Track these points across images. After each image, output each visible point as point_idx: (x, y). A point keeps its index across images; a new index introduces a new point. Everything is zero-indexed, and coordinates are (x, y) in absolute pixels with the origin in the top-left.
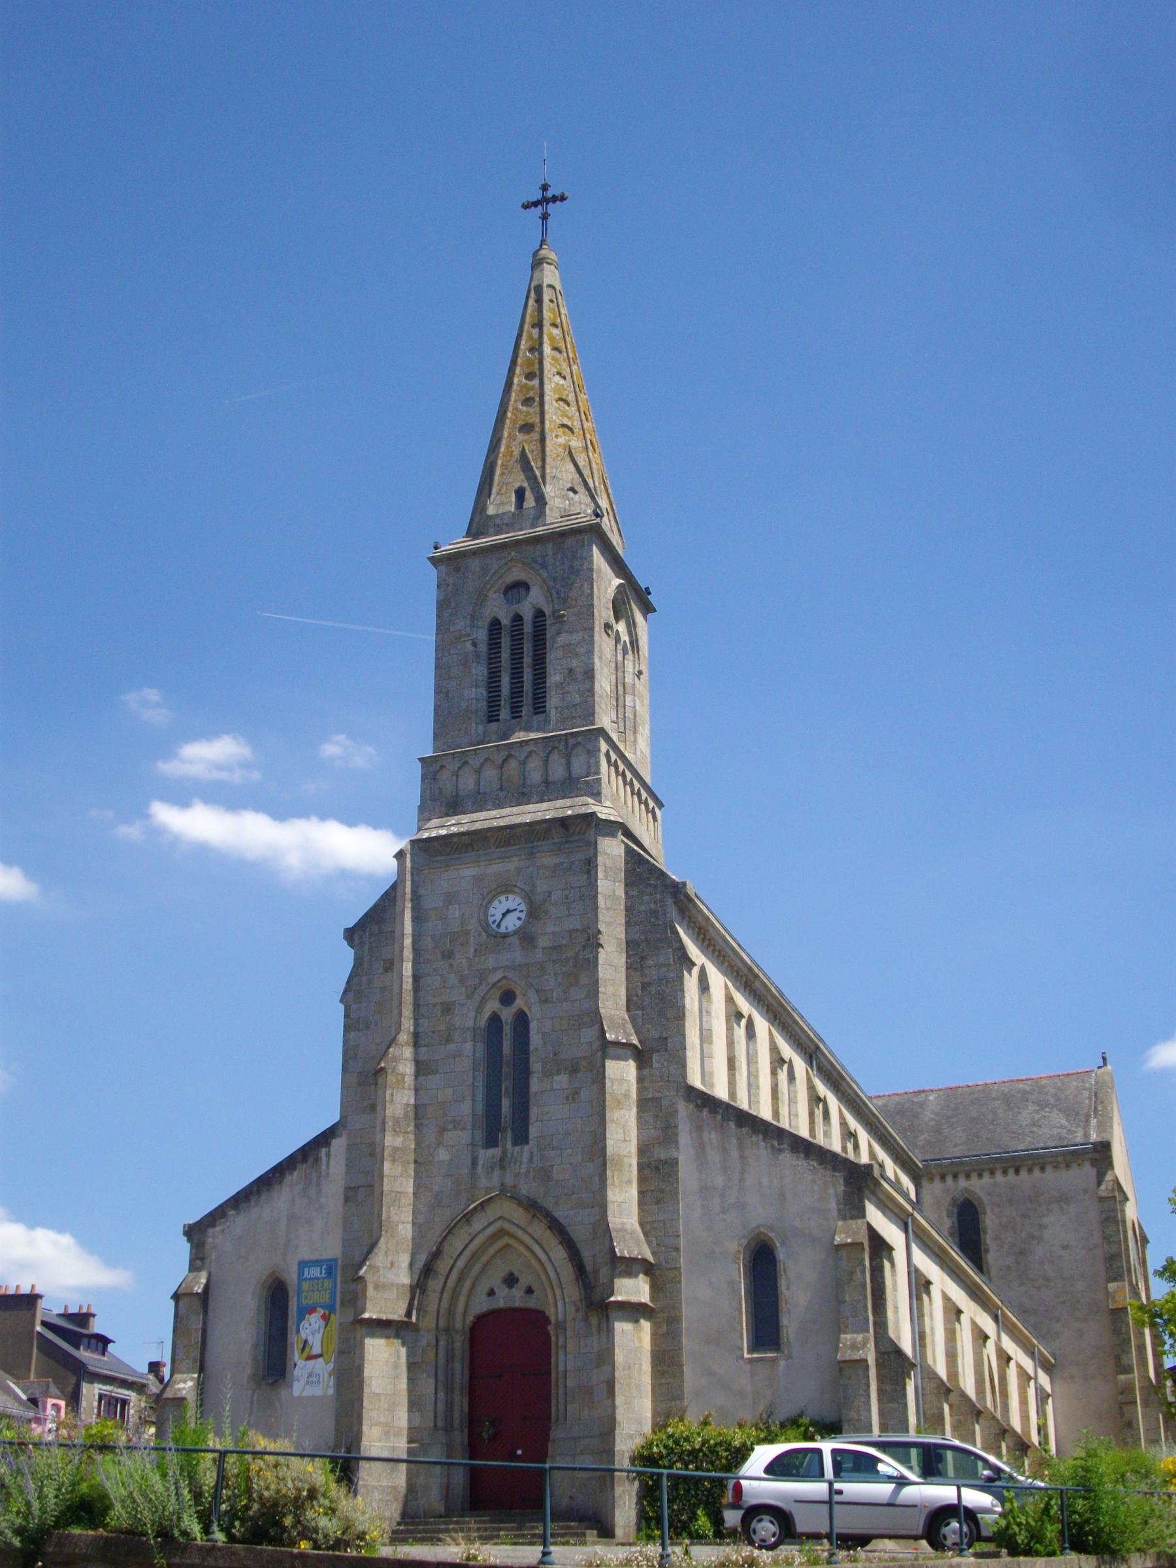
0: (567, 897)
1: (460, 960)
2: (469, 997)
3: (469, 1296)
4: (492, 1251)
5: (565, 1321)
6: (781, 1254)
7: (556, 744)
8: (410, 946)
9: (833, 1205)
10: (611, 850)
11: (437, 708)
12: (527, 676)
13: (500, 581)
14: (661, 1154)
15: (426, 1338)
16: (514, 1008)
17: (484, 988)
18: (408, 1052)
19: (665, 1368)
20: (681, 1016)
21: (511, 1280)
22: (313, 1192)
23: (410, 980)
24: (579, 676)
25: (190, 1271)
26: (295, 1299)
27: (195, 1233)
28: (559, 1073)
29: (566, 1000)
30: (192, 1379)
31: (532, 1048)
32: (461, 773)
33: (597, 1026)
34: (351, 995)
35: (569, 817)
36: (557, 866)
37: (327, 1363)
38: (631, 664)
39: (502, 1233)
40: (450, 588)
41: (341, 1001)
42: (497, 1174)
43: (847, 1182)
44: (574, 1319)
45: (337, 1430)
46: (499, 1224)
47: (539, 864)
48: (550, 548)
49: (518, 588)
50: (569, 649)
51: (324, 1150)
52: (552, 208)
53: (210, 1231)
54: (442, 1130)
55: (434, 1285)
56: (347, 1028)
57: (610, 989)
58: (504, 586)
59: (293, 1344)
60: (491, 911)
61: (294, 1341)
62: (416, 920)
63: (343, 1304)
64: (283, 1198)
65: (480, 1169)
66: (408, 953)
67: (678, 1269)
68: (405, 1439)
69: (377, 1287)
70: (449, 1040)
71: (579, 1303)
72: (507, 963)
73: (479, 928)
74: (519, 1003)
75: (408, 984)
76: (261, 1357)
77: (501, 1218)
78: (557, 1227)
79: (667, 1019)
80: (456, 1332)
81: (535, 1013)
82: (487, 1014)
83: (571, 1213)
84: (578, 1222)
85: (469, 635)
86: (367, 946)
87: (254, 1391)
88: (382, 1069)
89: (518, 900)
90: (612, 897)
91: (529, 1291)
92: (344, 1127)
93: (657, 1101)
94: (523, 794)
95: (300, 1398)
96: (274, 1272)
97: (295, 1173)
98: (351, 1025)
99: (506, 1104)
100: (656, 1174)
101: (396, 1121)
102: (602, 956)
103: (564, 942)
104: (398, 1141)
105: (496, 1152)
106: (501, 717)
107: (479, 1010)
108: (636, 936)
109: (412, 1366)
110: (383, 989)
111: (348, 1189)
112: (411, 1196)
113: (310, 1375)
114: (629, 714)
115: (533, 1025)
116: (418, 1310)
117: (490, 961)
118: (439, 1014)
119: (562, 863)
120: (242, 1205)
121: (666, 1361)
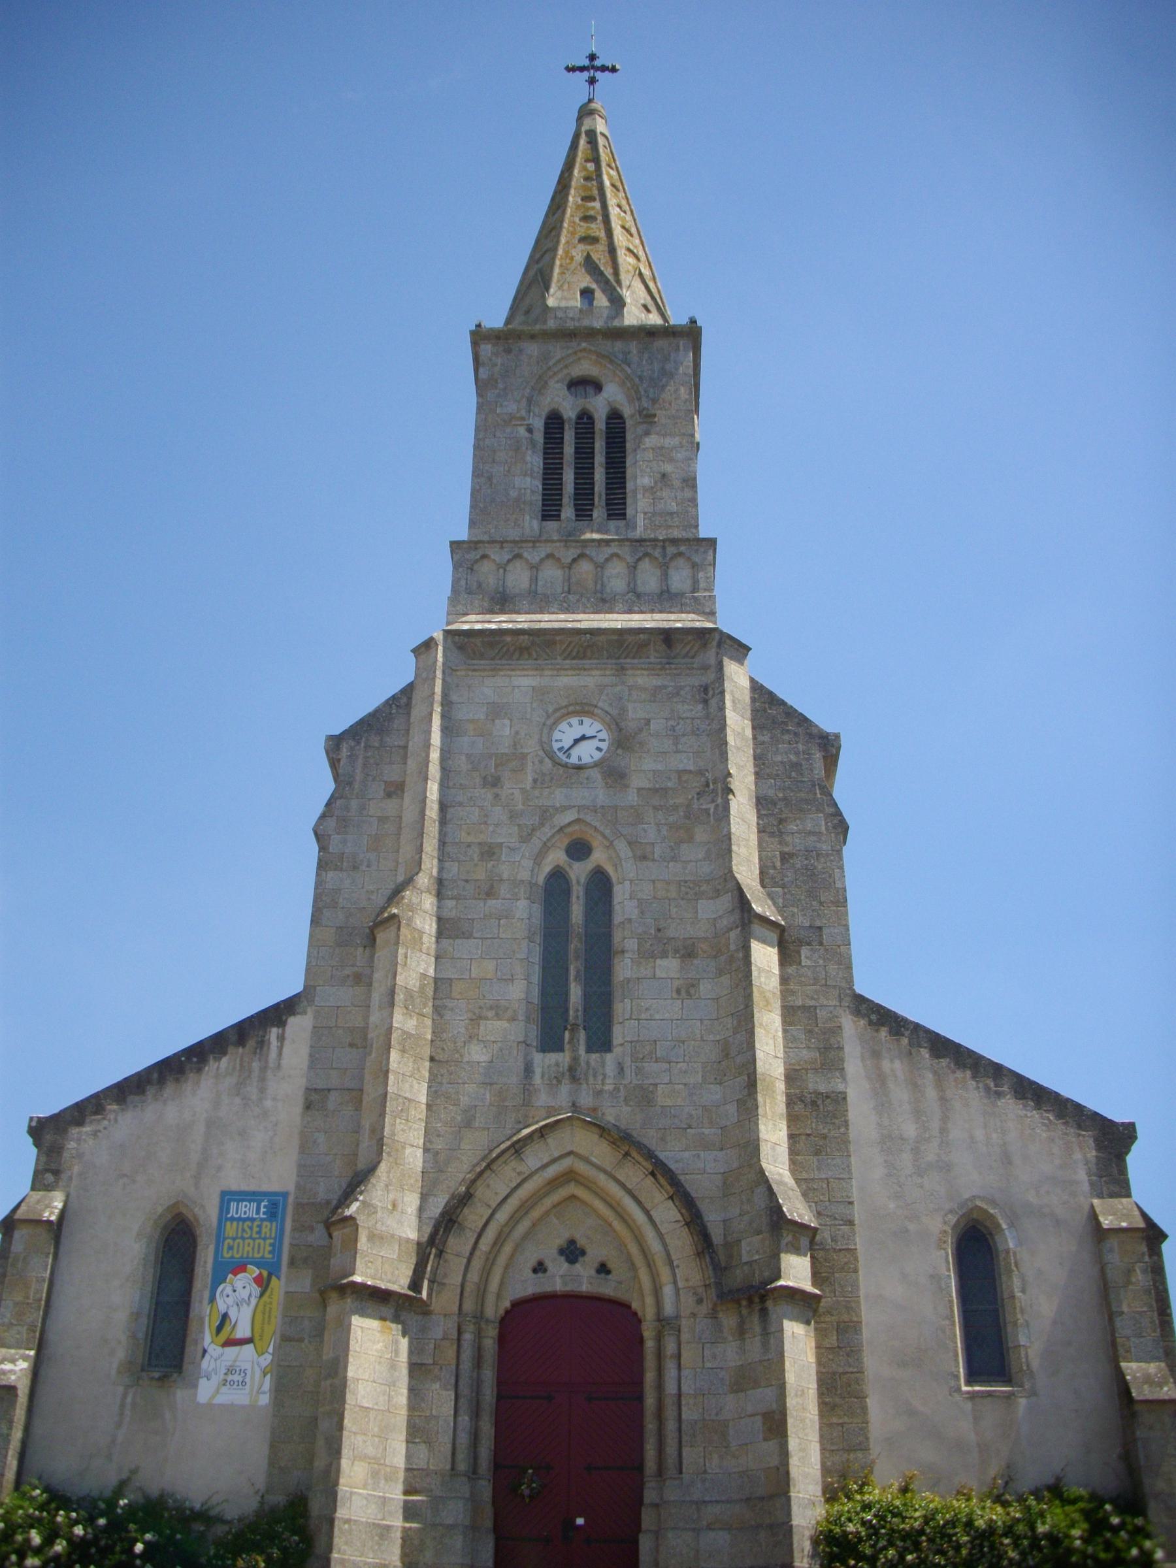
0: (673, 729)
1: (511, 789)
2: (525, 839)
3: (507, 1267)
4: (548, 1202)
5: (678, 1317)
6: (1009, 1240)
7: (650, 550)
8: (437, 763)
9: (1082, 1175)
11: (475, 493)
12: (599, 475)
13: (565, 371)
14: (816, 1083)
15: (441, 1328)
17: (547, 831)
18: (429, 902)
19: (837, 1400)
21: (572, 1252)
22: (252, 1090)
23: (436, 807)
24: (677, 483)
25: (33, 1188)
26: (212, 1248)
27: (48, 1133)
28: (664, 955)
29: (674, 859)
30: (25, 1358)
31: (617, 919)
32: (510, 567)
34: (331, 823)
35: (678, 629)
36: (657, 689)
37: (260, 1354)
39: (569, 1176)
40: (497, 369)
42: (565, 1088)
43: (1099, 1147)
44: (694, 1315)
45: (271, 1464)
46: (566, 1163)
47: (631, 682)
48: (634, 347)
49: (584, 385)
50: (662, 453)
51: (274, 1031)
53: (74, 1131)
54: (477, 1019)
55: (459, 1245)
56: (322, 865)
58: (568, 379)
59: (202, 1320)
60: (556, 735)
61: (204, 1313)
62: (447, 730)
63: (292, 1263)
64: (200, 1096)
65: (537, 1080)
66: (434, 770)
67: (852, 1251)
68: (400, 1487)
69: (372, 1237)
70: (490, 893)
71: (701, 1290)
72: (584, 802)
73: (541, 753)
74: (599, 857)
75: (432, 811)
76: (141, 1335)
77: (570, 1153)
78: (660, 1170)
79: (821, 903)
80: (487, 1321)
82: (547, 869)
83: (687, 1154)
84: (702, 1170)
85: (523, 419)
86: (360, 761)
87: (127, 1387)
88: (394, 916)
89: (598, 726)
90: (740, 735)
91: (603, 1269)
92: (311, 1002)
93: (810, 1011)
94: (604, 601)
95: (210, 1406)
96: (177, 1203)
97: (225, 1060)
99: (575, 993)
100: (817, 1114)
101: (409, 994)
103: (669, 784)
104: (411, 1024)
105: (563, 1059)
106: (563, 516)
107: (539, 858)
108: (771, 793)
109: (416, 1369)
110: (382, 820)
111: (309, 1090)
112: (424, 1107)
113: (230, 1371)
115: (620, 893)
116: (431, 1282)
117: (559, 796)
118: (476, 857)
119: (665, 687)
120: (130, 1098)
121: (840, 1389)
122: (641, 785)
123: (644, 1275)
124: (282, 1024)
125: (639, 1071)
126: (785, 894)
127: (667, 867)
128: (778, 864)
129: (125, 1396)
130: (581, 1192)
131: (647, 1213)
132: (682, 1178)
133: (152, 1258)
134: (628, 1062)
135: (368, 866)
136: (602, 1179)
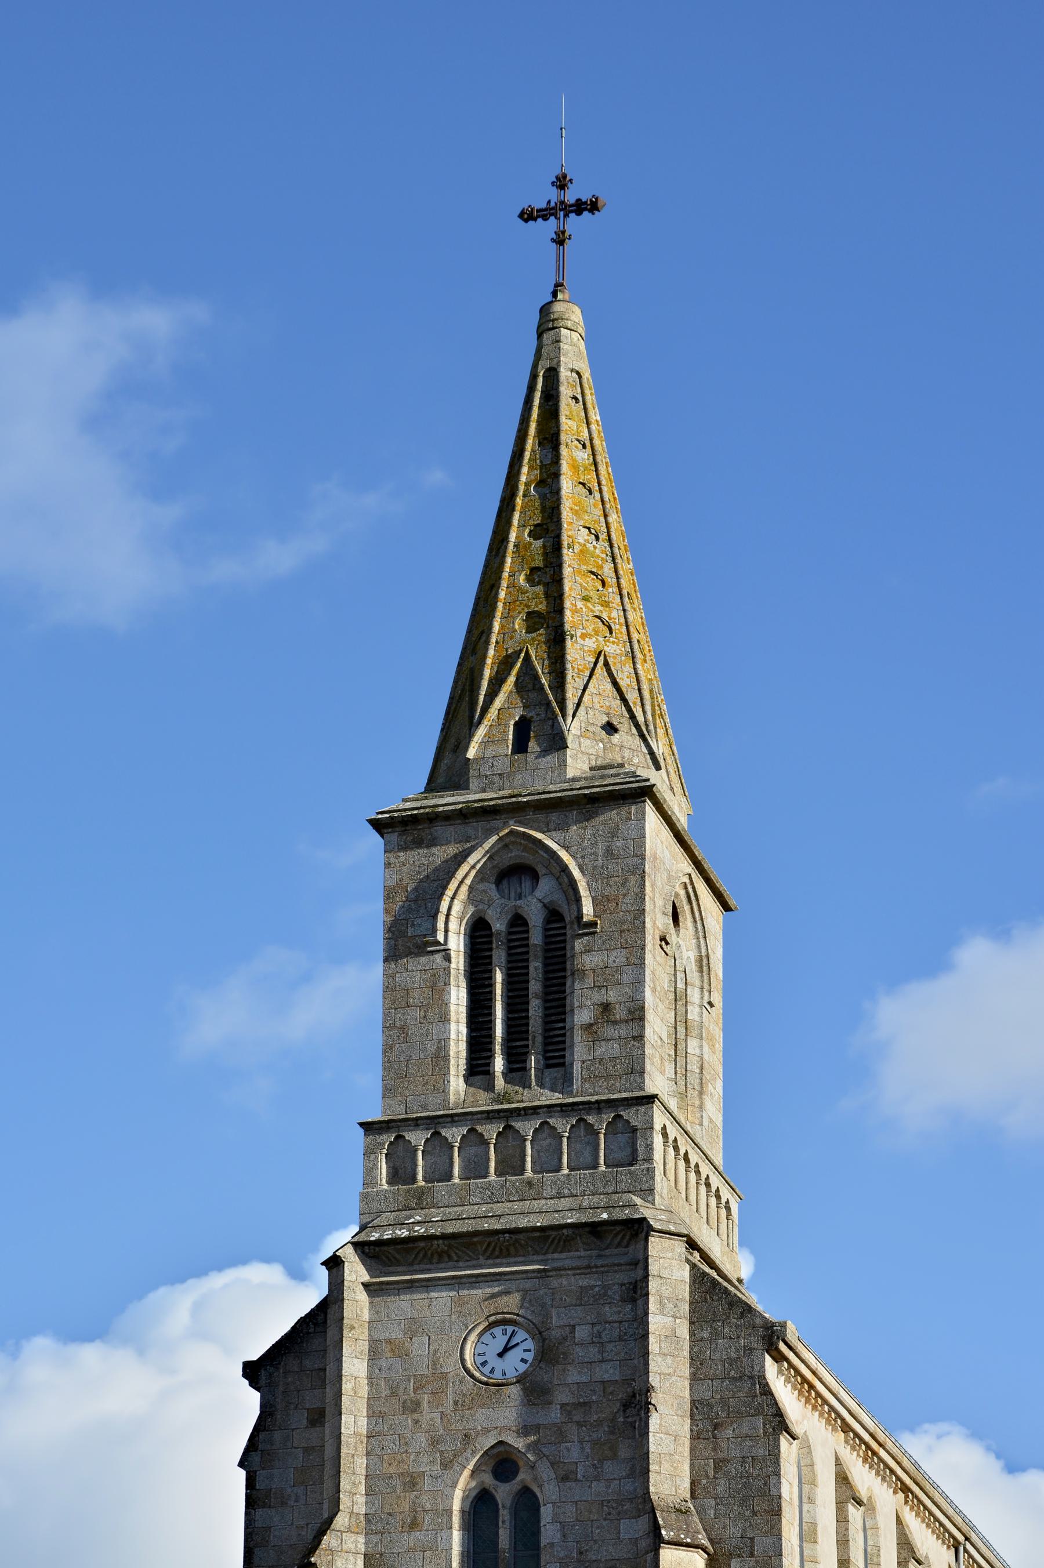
0: (599, 1334)
1: (429, 1415)
10: (668, 1270)
12: (535, 1008)
16: (514, 1485)
20: (775, 1512)
29: (597, 1479)
31: (543, 1542)
33: (645, 1519)
34: (256, 1458)
38: (697, 991)
41: (241, 1464)
50: (606, 977)
52: (574, 223)
57: (666, 1466)
70: (414, 1525)
81: (548, 1492)
98: (255, 1500)
102: (654, 1422)
108: (707, 1395)
110: (307, 1450)
114: (693, 1067)
115: (546, 1513)
117: (480, 1418)
119: (592, 1287)
122: (565, 1400)
126: (717, 1504)
127: (590, 1487)
128: (711, 1473)
135: (296, 1501)
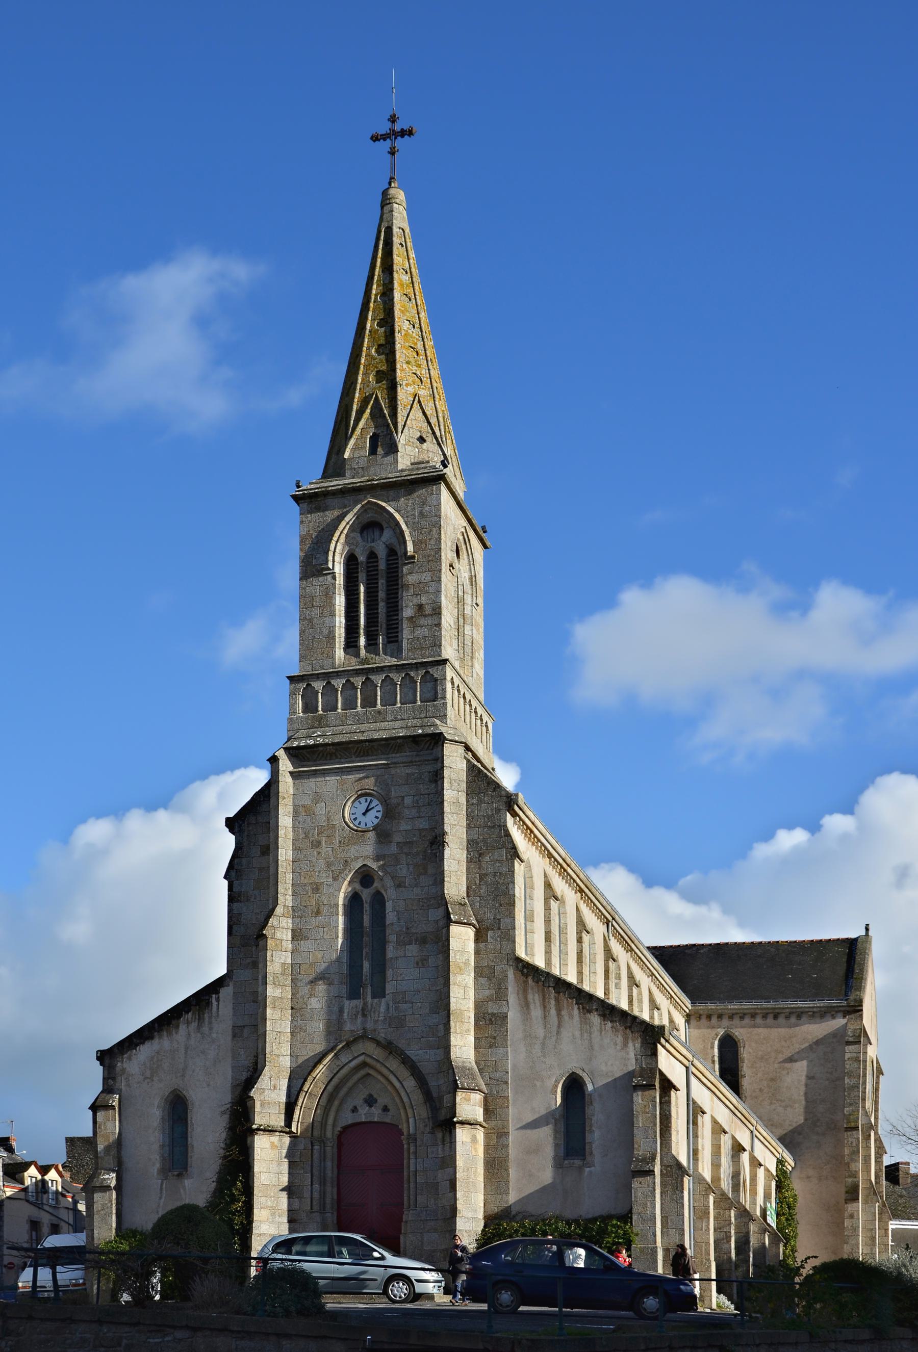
14: (492, 1008)
22: (205, 1029)
29: (416, 886)
34: (233, 873)
39: (364, 1064)
46: (362, 1058)
70: (318, 913)
76: (166, 1155)
78: (407, 1061)
83: (421, 1052)
87: (162, 1181)
99: (366, 966)
108: (476, 837)
110: (260, 869)
122: (399, 840)
123: (402, 1111)
124: (217, 993)
125: (397, 1009)
129: (162, 1185)
130: (372, 1072)
131: (401, 1083)
132: (418, 1064)
133: (166, 1117)
134: (391, 1004)
136: (378, 1066)
